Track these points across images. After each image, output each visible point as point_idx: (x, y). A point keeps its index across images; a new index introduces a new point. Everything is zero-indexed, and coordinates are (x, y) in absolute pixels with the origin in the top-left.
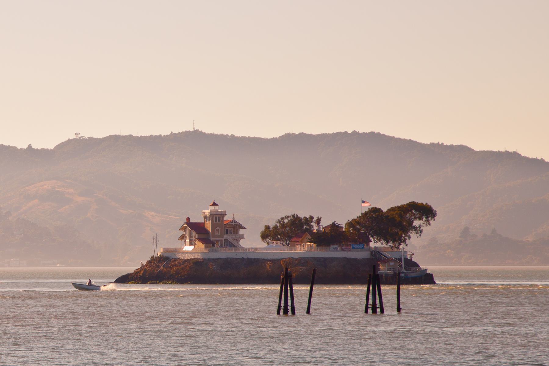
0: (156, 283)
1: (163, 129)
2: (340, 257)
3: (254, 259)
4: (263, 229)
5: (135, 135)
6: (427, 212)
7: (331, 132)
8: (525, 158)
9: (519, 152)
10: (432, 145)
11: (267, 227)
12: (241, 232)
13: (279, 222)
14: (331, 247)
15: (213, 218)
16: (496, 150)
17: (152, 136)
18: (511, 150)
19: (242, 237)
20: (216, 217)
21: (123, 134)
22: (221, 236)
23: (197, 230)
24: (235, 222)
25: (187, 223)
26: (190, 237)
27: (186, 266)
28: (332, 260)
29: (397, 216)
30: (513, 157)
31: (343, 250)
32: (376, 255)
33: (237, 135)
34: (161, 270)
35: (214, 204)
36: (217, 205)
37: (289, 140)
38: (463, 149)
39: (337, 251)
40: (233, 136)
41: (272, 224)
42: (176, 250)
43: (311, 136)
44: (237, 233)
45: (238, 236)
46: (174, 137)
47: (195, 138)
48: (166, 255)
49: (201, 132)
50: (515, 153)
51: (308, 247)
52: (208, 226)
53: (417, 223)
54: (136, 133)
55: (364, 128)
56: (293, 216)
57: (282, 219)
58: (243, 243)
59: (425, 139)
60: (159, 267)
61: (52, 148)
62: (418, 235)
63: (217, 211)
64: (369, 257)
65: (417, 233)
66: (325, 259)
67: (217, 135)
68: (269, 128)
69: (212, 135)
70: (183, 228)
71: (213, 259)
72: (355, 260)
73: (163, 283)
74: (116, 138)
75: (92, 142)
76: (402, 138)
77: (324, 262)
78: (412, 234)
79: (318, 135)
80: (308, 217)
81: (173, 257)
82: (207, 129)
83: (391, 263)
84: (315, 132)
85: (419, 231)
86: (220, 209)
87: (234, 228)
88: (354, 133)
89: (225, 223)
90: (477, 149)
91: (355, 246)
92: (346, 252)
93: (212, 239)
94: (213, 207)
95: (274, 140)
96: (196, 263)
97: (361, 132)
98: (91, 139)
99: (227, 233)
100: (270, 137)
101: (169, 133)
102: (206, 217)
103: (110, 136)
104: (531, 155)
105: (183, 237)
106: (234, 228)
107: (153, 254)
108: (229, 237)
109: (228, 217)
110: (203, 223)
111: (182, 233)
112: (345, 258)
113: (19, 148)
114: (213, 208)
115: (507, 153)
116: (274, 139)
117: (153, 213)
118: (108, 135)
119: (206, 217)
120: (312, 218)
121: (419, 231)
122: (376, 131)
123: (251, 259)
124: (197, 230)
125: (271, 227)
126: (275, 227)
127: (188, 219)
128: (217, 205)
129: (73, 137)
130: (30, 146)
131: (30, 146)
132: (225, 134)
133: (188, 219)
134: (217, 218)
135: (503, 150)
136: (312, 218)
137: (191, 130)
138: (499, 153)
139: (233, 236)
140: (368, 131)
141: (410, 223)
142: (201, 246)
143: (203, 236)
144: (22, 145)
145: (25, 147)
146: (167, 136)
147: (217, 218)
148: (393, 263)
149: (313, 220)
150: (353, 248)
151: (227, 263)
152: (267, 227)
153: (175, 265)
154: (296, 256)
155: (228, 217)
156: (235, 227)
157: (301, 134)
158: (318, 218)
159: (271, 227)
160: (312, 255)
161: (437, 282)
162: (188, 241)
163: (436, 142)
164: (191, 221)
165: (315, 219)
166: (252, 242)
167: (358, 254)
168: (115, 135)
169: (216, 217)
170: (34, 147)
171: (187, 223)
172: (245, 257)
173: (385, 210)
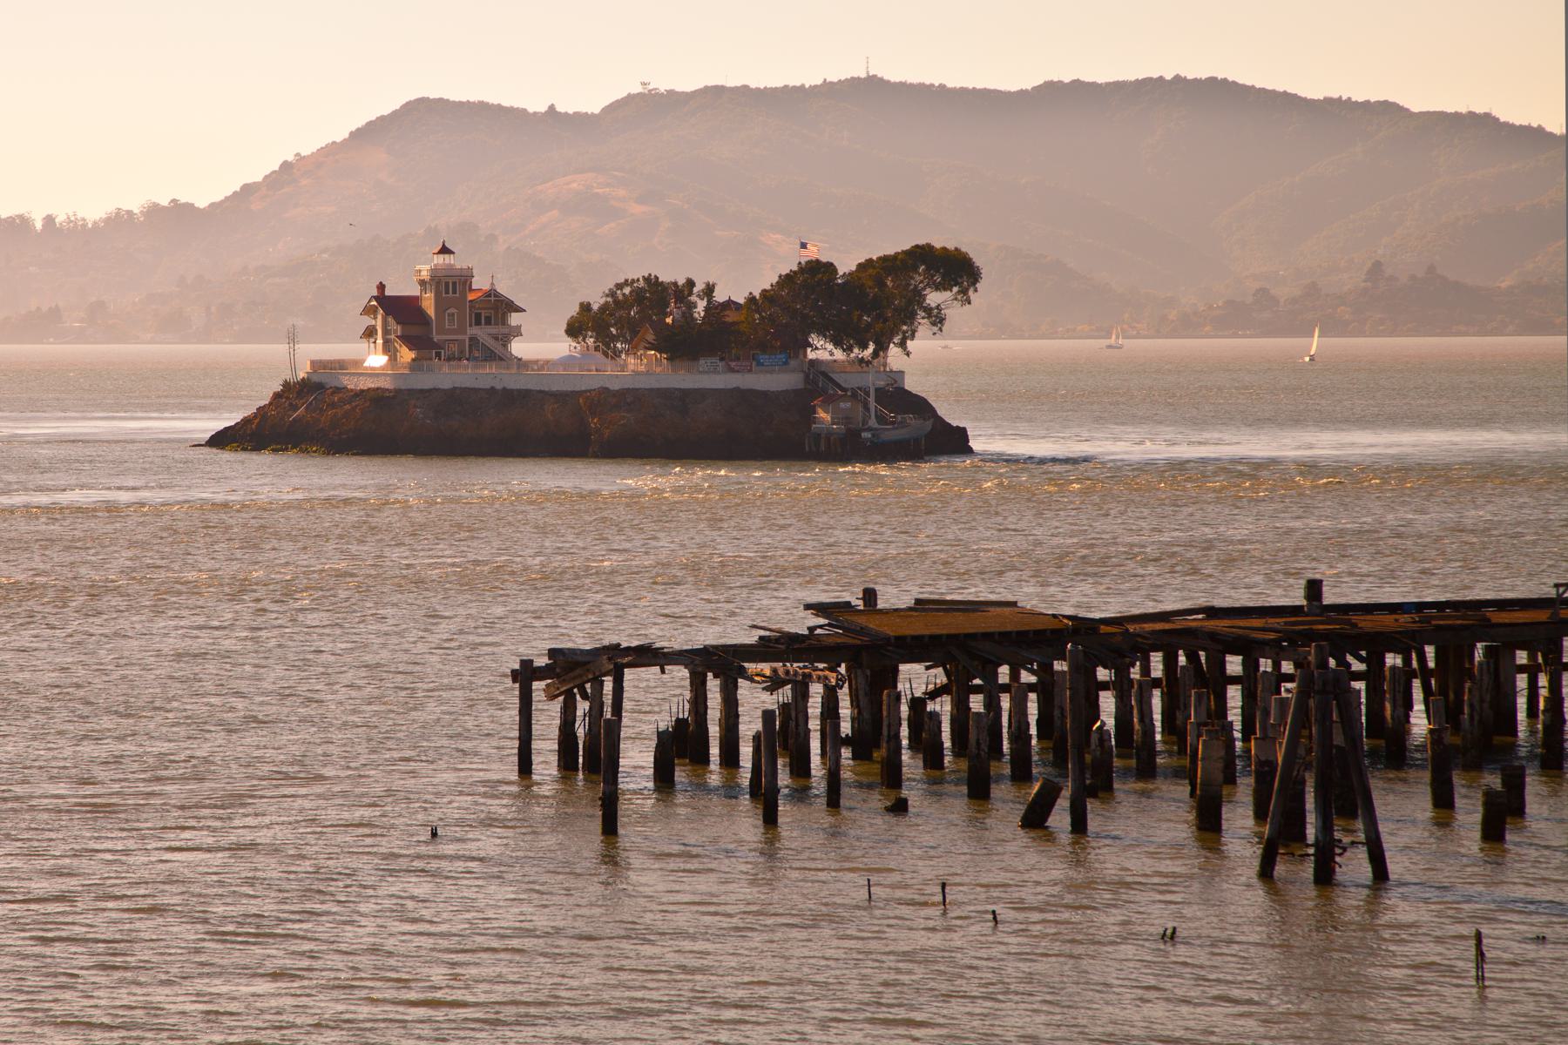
0: (286, 449)
1: (811, 77)
2: (721, 386)
3: (519, 391)
4: (574, 310)
5: (753, 86)
6: (956, 270)
7: (1132, 78)
8: (1506, 124)
9: (1496, 113)
10: (1329, 101)
11: (585, 307)
12: (514, 319)
13: (612, 294)
14: (702, 362)
15: (438, 283)
16: (1450, 109)
17: (786, 86)
18: (1479, 110)
19: (517, 332)
20: (447, 284)
21: (731, 83)
22: (462, 330)
23: (398, 314)
24: (497, 295)
25: (376, 298)
26: (386, 332)
27: (353, 409)
28: (702, 394)
29: (870, 283)
30: (1483, 123)
31: (732, 370)
32: (820, 381)
33: (950, 85)
34: (305, 418)
35: (445, 250)
36: (449, 252)
37: (1052, 92)
38: (1388, 109)
39: (715, 372)
40: (942, 87)
41: (597, 302)
42: (341, 365)
43: (1093, 85)
44: (504, 322)
45: (506, 331)
46: (828, 89)
47: (870, 88)
48: (315, 379)
49: (881, 79)
50: (1487, 115)
51: (650, 362)
52: (429, 305)
53: (933, 298)
54: (756, 82)
55: (1196, 70)
56: (647, 279)
57: (619, 286)
58: (519, 348)
59: (1313, 90)
60: (296, 408)
61: (597, 111)
62: (935, 329)
63: (451, 267)
64: (801, 386)
65: (934, 324)
66: (685, 393)
67: (911, 85)
68: (1014, 72)
69: (902, 85)
70: (368, 311)
71: (422, 391)
72: (765, 394)
73: (302, 451)
74: (717, 92)
75: (673, 99)
76: (1270, 88)
77: (683, 399)
78: (924, 326)
79: (1108, 84)
80: (681, 282)
81: (335, 384)
82: (893, 74)
83: (842, 405)
84: (1102, 78)
85: (937, 318)
86: (456, 262)
87: (496, 309)
88: (1177, 78)
89: (471, 297)
90: (1415, 109)
91: (763, 358)
92: (738, 376)
93: (436, 338)
94: (441, 256)
95: (1508, 126)
96: (377, 399)
97: (1190, 77)
98: (671, 93)
99: (478, 323)
100: (1014, 88)
101: (819, 82)
102: (422, 283)
103: (706, 88)
104: (1518, 120)
105: (369, 333)
106: (496, 309)
107: (288, 376)
108: (483, 333)
109: (480, 283)
110: (415, 299)
111: (368, 321)
112: (737, 389)
113: (531, 110)
114: (440, 260)
115: (1472, 114)
116: (1022, 93)
117: (778, 236)
118: (701, 86)
119: (422, 283)
120: (691, 283)
121: (937, 318)
122: (1220, 76)
123: (512, 391)
124: (398, 314)
125: (595, 307)
126: (604, 308)
127: (381, 287)
128: (449, 252)
129: (637, 89)
130: (552, 107)
131: (552, 107)
132: (928, 82)
133: (381, 287)
134: (451, 284)
135: (1464, 110)
136: (691, 283)
137: (863, 75)
138: (1457, 115)
139: (492, 330)
140: (1203, 74)
141: (918, 297)
142: (407, 355)
143: (415, 331)
144: (537, 105)
145: (543, 108)
146: (816, 86)
147: (451, 284)
148: (849, 405)
149: (695, 290)
150: (759, 364)
151: (455, 399)
152: (585, 307)
153: (333, 405)
154: (615, 386)
155: (480, 283)
156: (497, 308)
157: (1074, 82)
158: (708, 284)
159: (595, 307)
160: (653, 383)
161: (975, 444)
162: (380, 341)
163: (1336, 96)
164: (387, 293)
165: (699, 287)
166: (542, 345)
167: (774, 379)
168: (716, 87)
169: (447, 284)
170: (560, 108)
171: (376, 298)
172: (499, 387)
173: (846, 265)
